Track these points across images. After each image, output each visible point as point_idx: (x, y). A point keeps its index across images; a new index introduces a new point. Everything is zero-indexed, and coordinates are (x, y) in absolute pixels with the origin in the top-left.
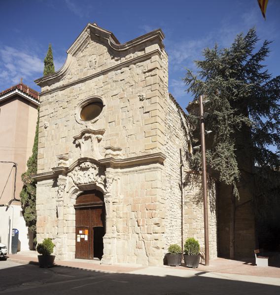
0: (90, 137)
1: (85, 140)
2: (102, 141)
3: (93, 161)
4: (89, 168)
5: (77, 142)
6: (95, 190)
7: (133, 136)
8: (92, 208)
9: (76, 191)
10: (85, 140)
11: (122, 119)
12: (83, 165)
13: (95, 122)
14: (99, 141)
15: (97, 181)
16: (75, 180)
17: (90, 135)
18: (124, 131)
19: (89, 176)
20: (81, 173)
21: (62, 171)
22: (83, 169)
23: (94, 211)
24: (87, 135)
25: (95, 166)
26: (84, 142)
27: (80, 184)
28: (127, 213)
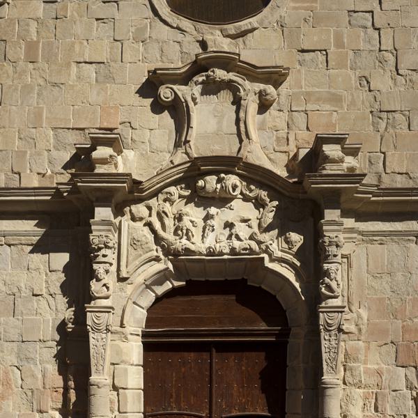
0: (231, 86)
1: (205, 92)
2: (273, 111)
3: (256, 176)
4: (234, 198)
5: (165, 93)
6: (244, 281)
7: (397, 115)
8: (224, 348)
9: (161, 277)
10: (205, 92)
11: (357, 52)
12: (211, 183)
13: (243, 34)
14: (264, 107)
15: (266, 251)
16: (169, 236)
17: (231, 76)
18: (363, 95)
19: (234, 228)
20: (195, 214)
21: (112, 191)
22: (201, 198)
23: (232, 359)
24: (220, 74)
25: (264, 194)
26: (197, 95)
27: (188, 251)
28: (379, 373)
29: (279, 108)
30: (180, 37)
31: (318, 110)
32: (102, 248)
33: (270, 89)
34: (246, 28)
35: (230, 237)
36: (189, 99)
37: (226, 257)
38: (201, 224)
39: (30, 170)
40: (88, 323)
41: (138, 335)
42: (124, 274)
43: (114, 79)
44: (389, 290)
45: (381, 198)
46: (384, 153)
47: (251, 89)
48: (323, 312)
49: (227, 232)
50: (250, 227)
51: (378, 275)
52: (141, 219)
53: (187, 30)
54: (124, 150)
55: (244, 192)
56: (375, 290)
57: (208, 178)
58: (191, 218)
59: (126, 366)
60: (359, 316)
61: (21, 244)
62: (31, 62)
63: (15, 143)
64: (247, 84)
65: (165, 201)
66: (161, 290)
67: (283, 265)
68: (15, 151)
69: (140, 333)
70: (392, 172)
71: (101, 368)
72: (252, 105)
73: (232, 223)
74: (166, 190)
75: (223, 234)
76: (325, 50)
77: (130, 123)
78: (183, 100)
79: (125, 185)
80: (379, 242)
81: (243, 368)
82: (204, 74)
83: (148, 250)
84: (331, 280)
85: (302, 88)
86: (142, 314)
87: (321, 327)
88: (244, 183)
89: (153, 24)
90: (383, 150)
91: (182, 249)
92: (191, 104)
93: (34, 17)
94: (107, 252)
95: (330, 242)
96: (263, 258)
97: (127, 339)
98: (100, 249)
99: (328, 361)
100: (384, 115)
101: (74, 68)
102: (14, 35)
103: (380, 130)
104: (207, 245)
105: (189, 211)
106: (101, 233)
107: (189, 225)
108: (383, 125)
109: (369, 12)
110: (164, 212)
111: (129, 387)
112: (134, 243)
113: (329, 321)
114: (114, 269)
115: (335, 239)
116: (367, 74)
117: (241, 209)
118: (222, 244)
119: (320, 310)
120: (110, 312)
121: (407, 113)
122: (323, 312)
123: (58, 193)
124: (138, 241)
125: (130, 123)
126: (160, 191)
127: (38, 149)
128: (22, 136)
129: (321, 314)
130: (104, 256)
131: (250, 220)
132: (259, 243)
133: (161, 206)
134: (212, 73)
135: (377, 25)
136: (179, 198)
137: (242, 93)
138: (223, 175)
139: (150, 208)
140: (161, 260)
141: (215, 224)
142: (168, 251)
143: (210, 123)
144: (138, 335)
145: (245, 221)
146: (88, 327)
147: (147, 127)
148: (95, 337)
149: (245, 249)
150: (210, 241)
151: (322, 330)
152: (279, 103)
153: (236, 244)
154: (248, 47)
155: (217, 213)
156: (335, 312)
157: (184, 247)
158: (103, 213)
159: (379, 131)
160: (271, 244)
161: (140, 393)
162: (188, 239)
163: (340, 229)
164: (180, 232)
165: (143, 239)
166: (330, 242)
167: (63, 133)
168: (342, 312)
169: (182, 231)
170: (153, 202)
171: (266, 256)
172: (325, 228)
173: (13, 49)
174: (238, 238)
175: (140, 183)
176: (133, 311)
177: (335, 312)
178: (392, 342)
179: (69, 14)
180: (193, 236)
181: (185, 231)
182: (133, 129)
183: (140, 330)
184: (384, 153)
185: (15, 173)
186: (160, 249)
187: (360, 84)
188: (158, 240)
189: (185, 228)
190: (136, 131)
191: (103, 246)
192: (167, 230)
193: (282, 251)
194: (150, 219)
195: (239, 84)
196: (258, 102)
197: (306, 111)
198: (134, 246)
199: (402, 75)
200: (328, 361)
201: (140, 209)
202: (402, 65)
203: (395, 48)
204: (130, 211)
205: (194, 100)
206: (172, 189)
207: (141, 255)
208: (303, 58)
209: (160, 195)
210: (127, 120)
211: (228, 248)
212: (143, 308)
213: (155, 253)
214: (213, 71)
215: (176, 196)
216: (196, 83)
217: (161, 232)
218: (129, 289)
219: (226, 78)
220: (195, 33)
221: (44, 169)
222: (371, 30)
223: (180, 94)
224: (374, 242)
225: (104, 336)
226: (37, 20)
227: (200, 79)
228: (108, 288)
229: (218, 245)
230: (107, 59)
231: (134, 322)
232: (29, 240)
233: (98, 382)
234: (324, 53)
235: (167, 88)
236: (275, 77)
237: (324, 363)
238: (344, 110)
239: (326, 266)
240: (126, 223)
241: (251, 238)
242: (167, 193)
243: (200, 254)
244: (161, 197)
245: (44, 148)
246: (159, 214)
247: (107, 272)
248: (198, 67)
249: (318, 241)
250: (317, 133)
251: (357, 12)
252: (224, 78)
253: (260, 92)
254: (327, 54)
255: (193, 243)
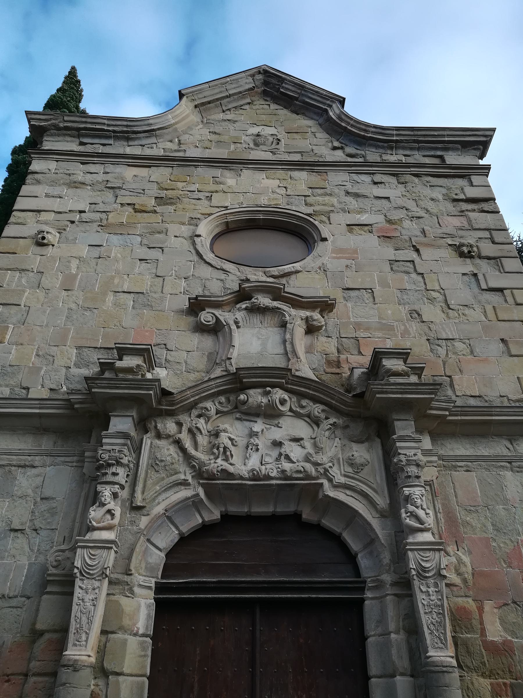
0: (275, 311)
5: (206, 317)
12: (255, 397)
14: (311, 330)
15: (326, 474)
20: (233, 430)
24: (264, 300)
27: (226, 474)
29: (327, 335)
30: (223, 276)
31: (370, 337)
32: (113, 465)
33: (316, 315)
34: (290, 270)
35: (278, 459)
36: (231, 322)
37: (274, 482)
38: (242, 442)
39: (42, 385)
40: (75, 564)
41: (150, 588)
42: (139, 502)
43: (152, 307)
44: (490, 528)
45: (459, 418)
46: (450, 377)
47: (296, 317)
48: (411, 550)
49: (275, 453)
50: (304, 447)
51: (472, 508)
52: (168, 437)
53: (231, 271)
54: (155, 368)
55: (294, 409)
56: (472, 527)
57: (251, 392)
58: (230, 435)
59: (127, 636)
60: (460, 561)
61: (11, 465)
62: (65, 290)
63: (31, 359)
64: (293, 312)
65: (199, 416)
66: (186, 527)
67: (348, 492)
68: (29, 367)
69: (153, 585)
70: (463, 395)
71: (84, 637)
72: (299, 330)
73: (280, 442)
74: (201, 405)
75: (270, 456)
76: (371, 289)
77: (165, 345)
78: (225, 324)
79: (151, 392)
80: (465, 469)
81: (301, 641)
82: (248, 302)
83: (172, 472)
84: (417, 507)
85: (350, 319)
86: (158, 558)
87: (414, 572)
88: (294, 399)
89: (197, 266)
90: (448, 374)
91: (218, 471)
92: (233, 327)
93: (76, 256)
94: (121, 471)
95: (407, 460)
96: (322, 484)
97: (132, 592)
98: (110, 465)
99: (432, 627)
100: (443, 343)
101: (110, 297)
102: (53, 269)
103: (441, 356)
104: (249, 468)
105: (228, 428)
106: (114, 447)
107: (229, 444)
108: (442, 352)
109: (409, 261)
110: (197, 428)
111: (126, 670)
112: (155, 464)
113: (423, 564)
114: (124, 494)
115: (414, 458)
116: (416, 307)
117: (291, 427)
118: (268, 466)
119: (408, 547)
120: (111, 548)
121: (467, 341)
122: (411, 550)
123: (69, 404)
124: (162, 461)
125: (165, 345)
126: (194, 405)
127: (55, 365)
128: (40, 353)
129: (410, 553)
130: (115, 474)
131: (302, 439)
132: (316, 464)
133: (194, 422)
134: (256, 301)
135: (420, 270)
136: (217, 414)
137: (288, 318)
138: (268, 389)
139: (180, 424)
140: (189, 484)
141: (260, 444)
142: (201, 474)
143: (252, 343)
144: (150, 588)
145: (297, 440)
146: (76, 571)
147: (184, 349)
148: (84, 587)
149: (299, 472)
150: (254, 462)
151: (415, 577)
152: (326, 330)
153: (287, 466)
154: (291, 286)
155: (263, 430)
156: (430, 550)
157: (220, 469)
158: (121, 423)
159: (439, 357)
160: (330, 467)
161: (143, 682)
162: (226, 460)
163: (414, 447)
164: (215, 451)
165: (169, 458)
166: (407, 460)
167: (89, 352)
168: (439, 550)
169: (218, 449)
170: (184, 418)
171: (325, 482)
172: (398, 444)
173: (49, 279)
174: (288, 458)
175: (170, 393)
176: (146, 551)
177: (430, 550)
178: (514, 602)
179: (113, 255)
180: (232, 456)
181: (221, 450)
182: (168, 350)
183: (153, 580)
184: (450, 377)
185: (24, 388)
186: (188, 471)
187: (411, 316)
188: (187, 457)
189: (222, 446)
190: (172, 353)
191: (114, 462)
192: (201, 448)
193: (345, 476)
194: (180, 436)
195: (284, 311)
196: (305, 327)
197: (356, 337)
198: (156, 467)
199: (452, 309)
200: (432, 627)
201: (169, 426)
202: (453, 302)
203: (442, 288)
204: (156, 427)
205: (236, 323)
206: (208, 404)
207: (163, 479)
208: (348, 295)
209: (193, 411)
210: (163, 342)
211: (275, 471)
212: (160, 550)
213: (183, 477)
214: (257, 299)
215: (213, 411)
216: (239, 310)
217: (192, 451)
218: (144, 522)
219: (270, 305)
220: (238, 274)
221: (55, 370)
222: (414, 275)
223: (222, 319)
224: (458, 469)
225: (97, 584)
226: (79, 258)
227: (244, 306)
228: (113, 516)
229: (263, 467)
230: (147, 290)
231: (146, 568)
232: (21, 460)
233: (76, 660)
234: (370, 291)
235: (208, 313)
236: (325, 306)
237: (426, 631)
238: (398, 337)
239: (407, 491)
240: (149, 442)
241: (307, 459)
242: (202, 408)
243: (242, 478)
244: (195, 412)
245: (63, 364)
246: (190, 431)
247: (115, 495)
248: (242, 295)
249: (391, 461)
250: (376, 347)
251: (398, 261)
252: (268, 305)
253: (307, 317)
254: (373, 292)
255: (231, 464)
